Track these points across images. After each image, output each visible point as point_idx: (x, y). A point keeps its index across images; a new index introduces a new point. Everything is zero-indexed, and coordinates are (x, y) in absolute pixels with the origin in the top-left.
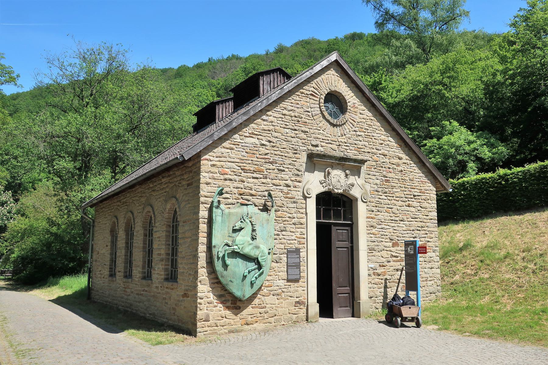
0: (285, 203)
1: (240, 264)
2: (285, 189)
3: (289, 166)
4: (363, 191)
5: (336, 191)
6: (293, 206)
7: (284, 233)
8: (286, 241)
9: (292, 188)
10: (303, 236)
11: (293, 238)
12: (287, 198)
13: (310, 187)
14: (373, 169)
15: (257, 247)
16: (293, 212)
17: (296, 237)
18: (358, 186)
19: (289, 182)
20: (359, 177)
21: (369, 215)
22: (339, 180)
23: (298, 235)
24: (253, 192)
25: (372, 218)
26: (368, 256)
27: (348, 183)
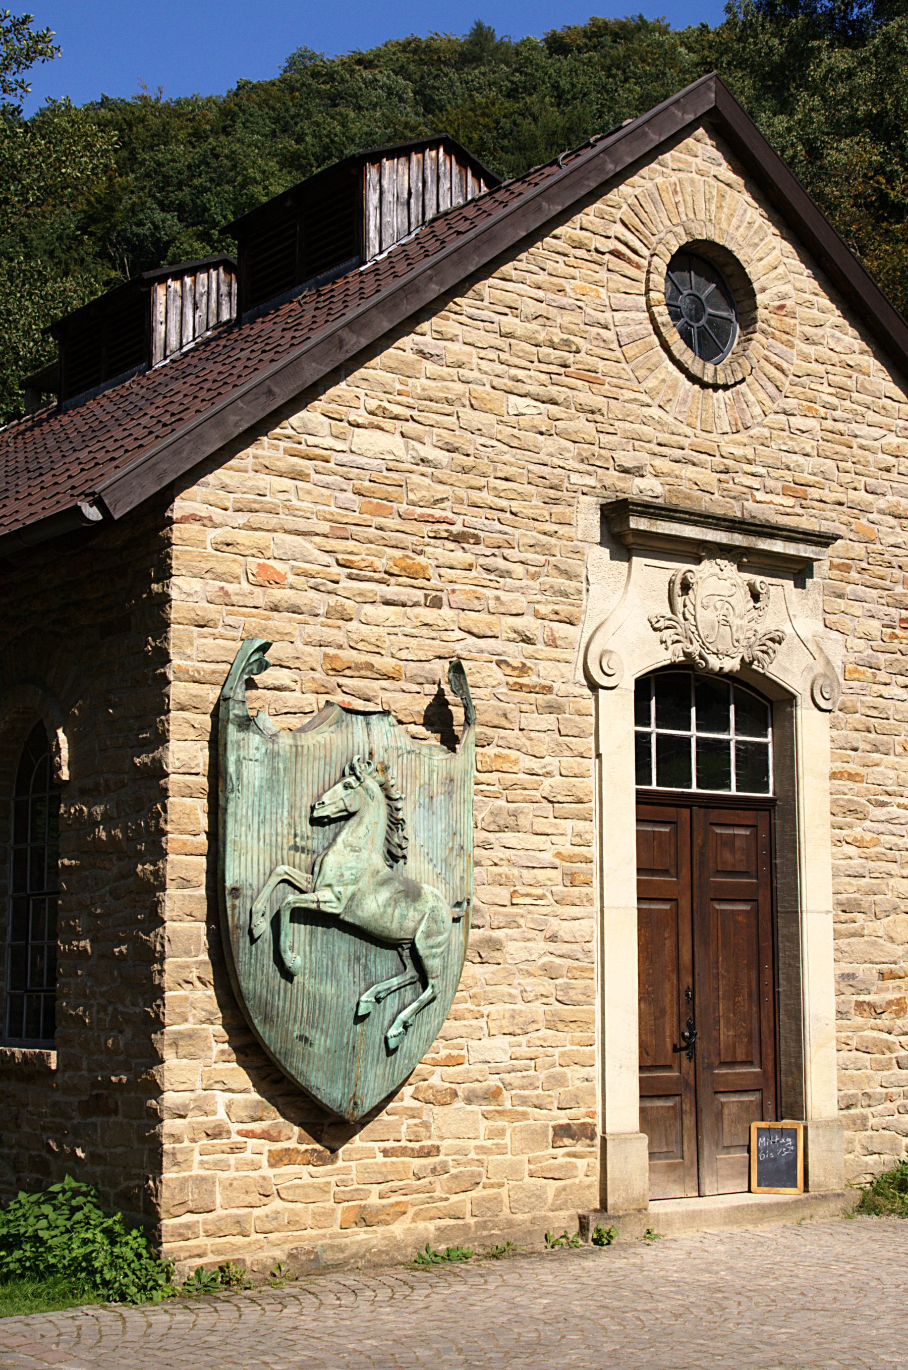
1: (342, 968)
2: (515, 653)
3: (529, 556)
4: (819, 668)
5: (715, 663)
7: (509, 838)
8: (515, 871)
11: (547, 857)
12: (520, 687)
14: (854, 575)
15: (412, 893)
16: (542, 750)
17: (558, 855)
19: (528, 624)
21: (839, 766)
22: (727, 617)
24: (384, 663)
25: (851, 777)
26: (837, 935)
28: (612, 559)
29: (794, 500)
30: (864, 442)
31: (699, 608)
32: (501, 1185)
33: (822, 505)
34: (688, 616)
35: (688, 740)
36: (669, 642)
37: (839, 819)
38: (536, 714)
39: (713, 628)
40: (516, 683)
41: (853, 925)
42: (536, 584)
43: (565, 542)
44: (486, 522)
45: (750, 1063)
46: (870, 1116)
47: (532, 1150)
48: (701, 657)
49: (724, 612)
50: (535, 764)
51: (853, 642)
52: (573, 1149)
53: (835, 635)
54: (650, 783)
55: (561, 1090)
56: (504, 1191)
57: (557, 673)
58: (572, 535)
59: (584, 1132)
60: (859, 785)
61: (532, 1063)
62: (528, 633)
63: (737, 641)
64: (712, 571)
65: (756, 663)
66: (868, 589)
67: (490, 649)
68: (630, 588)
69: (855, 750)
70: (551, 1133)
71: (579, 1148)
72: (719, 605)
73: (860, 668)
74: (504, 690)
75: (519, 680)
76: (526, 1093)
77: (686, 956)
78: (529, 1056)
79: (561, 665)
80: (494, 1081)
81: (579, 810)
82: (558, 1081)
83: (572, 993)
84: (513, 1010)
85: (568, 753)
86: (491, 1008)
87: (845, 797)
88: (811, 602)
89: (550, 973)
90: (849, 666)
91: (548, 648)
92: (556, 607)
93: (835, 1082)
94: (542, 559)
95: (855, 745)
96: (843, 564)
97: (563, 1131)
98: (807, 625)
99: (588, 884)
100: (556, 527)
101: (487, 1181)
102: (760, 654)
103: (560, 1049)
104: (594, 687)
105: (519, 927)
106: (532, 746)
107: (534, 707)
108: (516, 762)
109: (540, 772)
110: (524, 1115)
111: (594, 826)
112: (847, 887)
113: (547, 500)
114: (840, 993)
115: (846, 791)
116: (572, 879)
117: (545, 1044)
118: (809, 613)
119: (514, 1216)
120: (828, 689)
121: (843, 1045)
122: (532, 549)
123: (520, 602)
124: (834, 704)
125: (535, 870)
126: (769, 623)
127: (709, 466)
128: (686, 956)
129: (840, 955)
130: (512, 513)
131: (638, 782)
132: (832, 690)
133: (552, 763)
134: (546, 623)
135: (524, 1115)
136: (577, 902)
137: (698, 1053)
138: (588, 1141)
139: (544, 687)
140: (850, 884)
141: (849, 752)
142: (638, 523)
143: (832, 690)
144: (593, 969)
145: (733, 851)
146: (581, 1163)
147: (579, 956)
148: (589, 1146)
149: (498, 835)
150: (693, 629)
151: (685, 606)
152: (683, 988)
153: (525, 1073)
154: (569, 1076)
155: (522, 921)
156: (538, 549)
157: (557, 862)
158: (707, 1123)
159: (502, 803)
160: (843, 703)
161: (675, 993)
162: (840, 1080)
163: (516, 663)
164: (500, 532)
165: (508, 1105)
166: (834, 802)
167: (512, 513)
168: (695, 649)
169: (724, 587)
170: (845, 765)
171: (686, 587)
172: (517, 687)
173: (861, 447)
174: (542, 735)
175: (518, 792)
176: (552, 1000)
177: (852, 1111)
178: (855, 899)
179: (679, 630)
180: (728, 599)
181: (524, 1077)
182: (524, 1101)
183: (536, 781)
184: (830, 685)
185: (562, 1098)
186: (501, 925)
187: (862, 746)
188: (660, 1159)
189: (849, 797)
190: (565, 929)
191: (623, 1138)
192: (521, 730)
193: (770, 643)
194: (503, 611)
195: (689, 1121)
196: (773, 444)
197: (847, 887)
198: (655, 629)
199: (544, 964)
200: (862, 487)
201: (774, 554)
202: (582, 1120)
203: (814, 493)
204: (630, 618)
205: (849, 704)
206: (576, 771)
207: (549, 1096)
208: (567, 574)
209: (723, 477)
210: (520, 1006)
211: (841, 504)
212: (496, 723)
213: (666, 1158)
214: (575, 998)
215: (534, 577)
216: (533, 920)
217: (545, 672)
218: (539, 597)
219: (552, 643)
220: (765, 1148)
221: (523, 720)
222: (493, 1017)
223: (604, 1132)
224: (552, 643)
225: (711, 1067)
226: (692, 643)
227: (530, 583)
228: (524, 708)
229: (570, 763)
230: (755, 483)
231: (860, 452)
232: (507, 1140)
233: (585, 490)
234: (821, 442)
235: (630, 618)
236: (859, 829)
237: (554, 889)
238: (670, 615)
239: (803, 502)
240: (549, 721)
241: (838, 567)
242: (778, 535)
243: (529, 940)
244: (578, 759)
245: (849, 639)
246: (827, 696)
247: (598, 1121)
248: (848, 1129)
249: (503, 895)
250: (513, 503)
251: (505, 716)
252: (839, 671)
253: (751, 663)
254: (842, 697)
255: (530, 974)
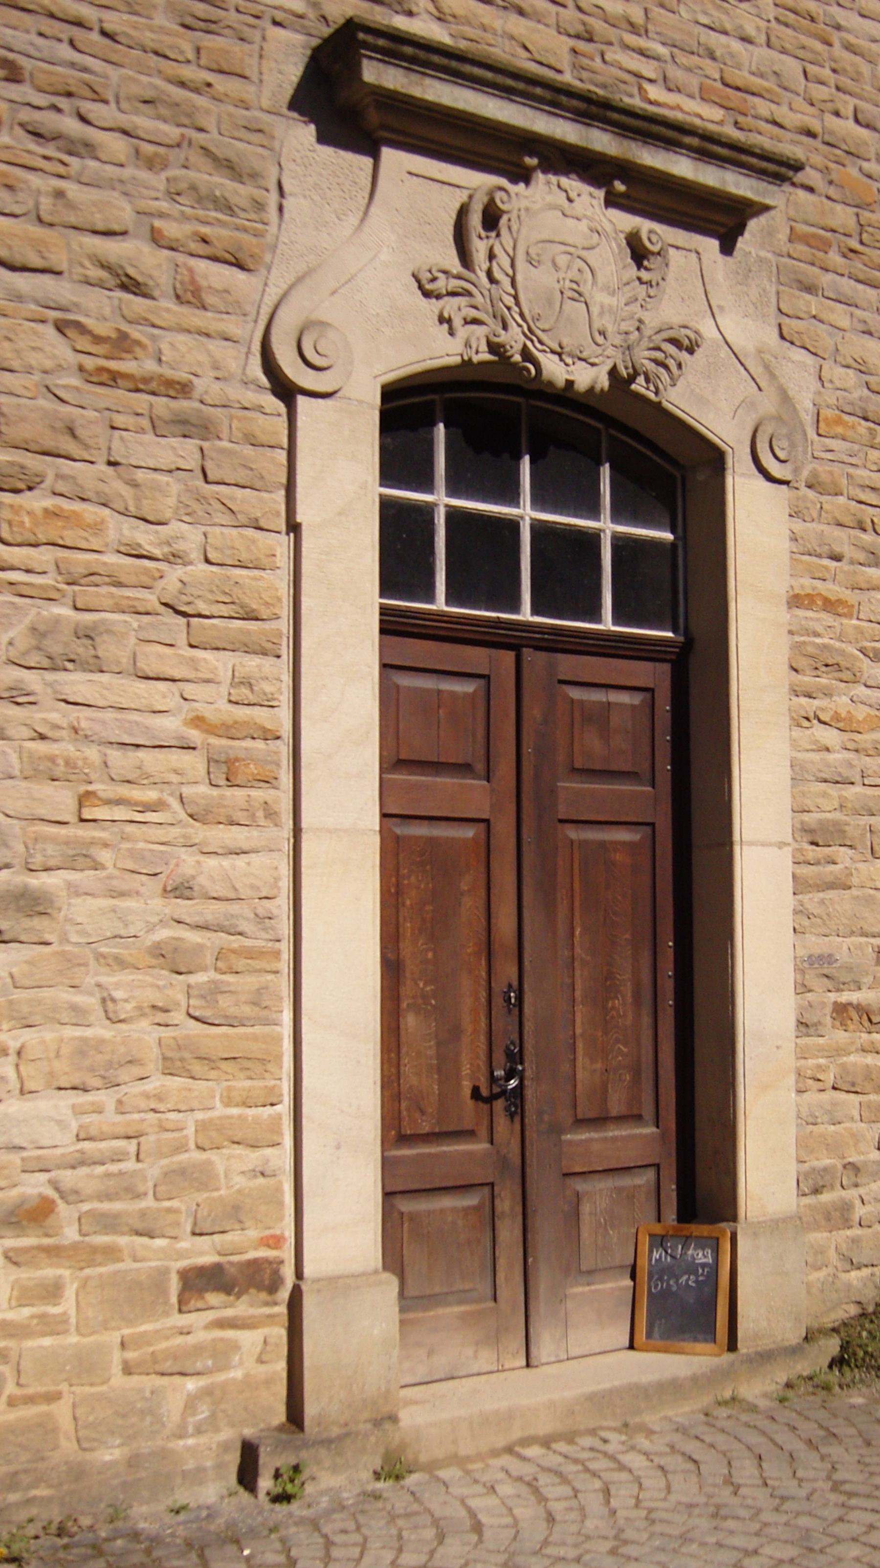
0: (89, 421)
2: (101, 309)
3: (143, 122)
4: (768, 404)
5: (555, 370)
6: (166, 459)
7: (77, 684)
8: (92, 753)
9: (166, 308)
10: (259, 714)
11: (170, 726)
12: (113, 379)
13: (328, 310)
14: (834, 258)
16: (166, 506)
17: (198, 721)
18: (722, 340)
19: (136, 254)
20: (727, 248)
21: (806, 584)
22: (578, 288)
23: (215, 703)
25: (830, 605)
26: (800, 885)
27: (652, 320)
28: (295, 104)
29: (722, 112)
30: (851, 39)
31: (521, 263)
32: (52, 1397)
33: (776, 130)
34: (498, 274)
35: (513, 526)
36: (457, 322)
37: (807, 680)
38: (149, 437)
39: (550, 303)
40: (101, 370)
41: (832, 867)
42: (158, 181)
43: (231, 109)
44: (40, 41)
45: (637, 1118)
46: (858, 1202)
47: (131, 1323)
48: (526, 354)
49: (573, 274)
50: (145, 537)
51: (835, 373)
52: (229, 1313)
53: (799, 355)
54: (430, 597)
55: (201, 1197)
56: (62, 1412)
57: (203, 358)
58: (245, 96)
59: (258, 1277)
60: (845, 621)
61: (132, 1146)
62: (131, 271)
63: (602, 333)
64: (549, 199)
65: (641, 380)
66: (861, 287)
67: (39, 295)
68: (373, 209)
69: (837, 558)
70: (174, 1285)
71: (242, 1308)
72: (562, 260)
73: (846, 418)
74: (75, 381)
75: (113, 365)
76: (117, 1206)
77: (505, 924)
78: (121, 1130)
79: (215, 346)
80: (35, 1186)
81: (248, 632)
82: (198, 1178)
83: (224, 1002)
84: (84, 1040)
85: (226, 519)
86: (27, 1036)
87: (818, 640)
88: (754, 292)
89: (172, 960)
90: (826, 413)
91: (184, 309)
92: (205, 230)
93: (793, 1150)
94: (172, 132)
95: (837, 549)
96: (814, 236)
97: (202, 1281)
98: (742, 327)
99: (268, 781)
100: (210, 77)
101: (19, 1392)
102: (651, 367)
103: (200, 1115)
104: (286, 391)
105: (97, 866)
106: (138, 499)
107: (145, 423)
108: (98, 528)
109: (157, 552)
110: (111, 1253)
111: (284, 665)
112: (820, 801)
113: (189, 21)
114: (802, 988)
115: (819, 629)
116: (227, 771)
117: (161, 1107)
118: (751, 310)
119: (88, 1456)
120: (785, 443)
121: (806, 1081)
122: (145, 108)
123: (123, 213)
124: (796, 471)
125: (141, 754)
126: (671, 310)
127: (552, 21)
128: (505, 924)
129: (806, 922)
130: (104, 33)
131: (387, 586)
132: (793, 445)
133: (190, 539)
134: (181, 258)
135: (111, 1253)
136: (241, 817)
137: (528, 1106)
138: (263, 1296)
139: (170, 383)
140: (825, 795)
141: (826, 562)
142: (377, 74)
143: (793, 445)
144: (277, 954)
145: (605, 733)
146: (250, 1339)
147: (244, 926)
148: (266, 1304)
149: (50, 676)
150: (510, 301)
151: (491, 256)
152: (499, 987)
153: (114, 1168)
154: (220, 1169)
155: (105, 856)
156: (163, 111)
157: (195, 735)
158: (546, 1230)
159: (64, 611)
160: (814, 474)
161: (483, 994)
162: (802, 1143)
163: (103, 329)
164: (73, 65)
165: (71, 1234)
166: (797, 647)
167: (104, 33)
168: (513, 339)
169: (575, 232)
170: (817, 583)
171: (492, 219)
172: (105, 377)
173: (848, 47)
174: (164, 478)
175: (104, 590)
176: (178, 1017)
177: (826, 1197)
178: (836, 823)
179: (479, 300)
180: (583, 253)
181: (108, 1175)
182: (110, 1223)
183: (147, 571)
184: (789, 437)
185: (203, 1212)
186: (52, 863)
187: (847, 550)
188: (449, 1304)
189: (826, 641)
190: (210, 871)
191: (340, 1284)
192: (110, 463)
193: (671, 349)
194: (73, 220)
195: (509, 1233)
196: (682, 9)
197: (820, 801)
198: (427, 294)
199: (157, 945)
200: (850, 114)
201: (681, 188)
202: (251, 1255)
203: (763, 107)
204: (372, 268)
205: (824, 477)
206: (244, 556)
207: (169, 1210)
208: (230, 167)
209: (581, 46)
210: (100, 1031)
211: (810, 134)
212: (49, 443)
213: (461, 1302)
214: (232, 1011)
215: (151, 164)
216: (133, 854)
217: (179, 353)
218: (164, 205)
219: (190, 295)
220: (662, 1272)
221: (116, 444)
222: (29, 1054)
223: (299, 1274)
224: (190, 295)
225: (557, 1130)
226: (505, 327)
227: (144, 175)
228: (120, 420)
229: (228, 537)
230: (648, 69)
231: (846, 55)
232: (67, 1305)
233: (280, 16)
234: (774, 24)
235: (372, 268)
236: (845, 699)
237: (186, 790)
238: (455, 266)
239: (741, 119)
240: (186, 451)
241: (806, 240)
242: (679, 145)
243: (122, 894)
244: (250, 532)
245: (826, 366)
246: (782, 455)
247: (288, 1254)
248: (817, 1227)
249: (61, 800)
250: (107, 15)
251: (71, 431)
252: (808, 419)
253: (632, 379)
254: (815, 465)
255: (121, 963)
